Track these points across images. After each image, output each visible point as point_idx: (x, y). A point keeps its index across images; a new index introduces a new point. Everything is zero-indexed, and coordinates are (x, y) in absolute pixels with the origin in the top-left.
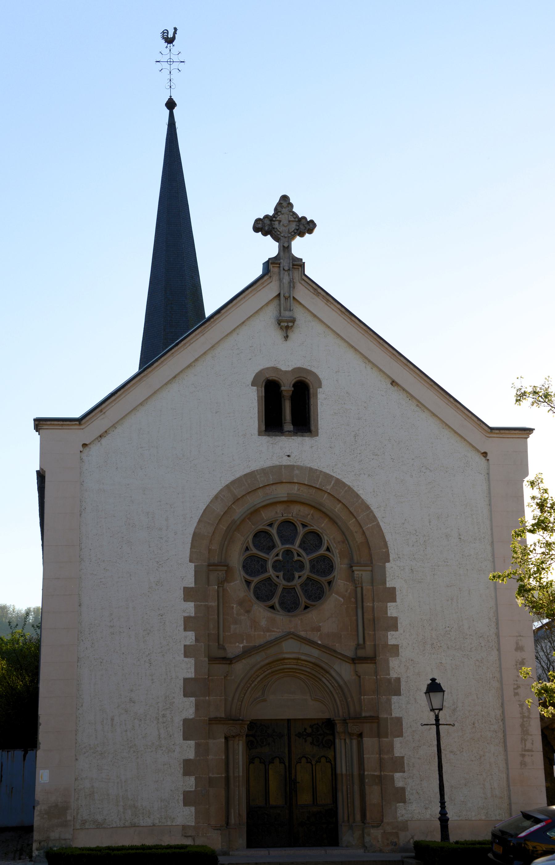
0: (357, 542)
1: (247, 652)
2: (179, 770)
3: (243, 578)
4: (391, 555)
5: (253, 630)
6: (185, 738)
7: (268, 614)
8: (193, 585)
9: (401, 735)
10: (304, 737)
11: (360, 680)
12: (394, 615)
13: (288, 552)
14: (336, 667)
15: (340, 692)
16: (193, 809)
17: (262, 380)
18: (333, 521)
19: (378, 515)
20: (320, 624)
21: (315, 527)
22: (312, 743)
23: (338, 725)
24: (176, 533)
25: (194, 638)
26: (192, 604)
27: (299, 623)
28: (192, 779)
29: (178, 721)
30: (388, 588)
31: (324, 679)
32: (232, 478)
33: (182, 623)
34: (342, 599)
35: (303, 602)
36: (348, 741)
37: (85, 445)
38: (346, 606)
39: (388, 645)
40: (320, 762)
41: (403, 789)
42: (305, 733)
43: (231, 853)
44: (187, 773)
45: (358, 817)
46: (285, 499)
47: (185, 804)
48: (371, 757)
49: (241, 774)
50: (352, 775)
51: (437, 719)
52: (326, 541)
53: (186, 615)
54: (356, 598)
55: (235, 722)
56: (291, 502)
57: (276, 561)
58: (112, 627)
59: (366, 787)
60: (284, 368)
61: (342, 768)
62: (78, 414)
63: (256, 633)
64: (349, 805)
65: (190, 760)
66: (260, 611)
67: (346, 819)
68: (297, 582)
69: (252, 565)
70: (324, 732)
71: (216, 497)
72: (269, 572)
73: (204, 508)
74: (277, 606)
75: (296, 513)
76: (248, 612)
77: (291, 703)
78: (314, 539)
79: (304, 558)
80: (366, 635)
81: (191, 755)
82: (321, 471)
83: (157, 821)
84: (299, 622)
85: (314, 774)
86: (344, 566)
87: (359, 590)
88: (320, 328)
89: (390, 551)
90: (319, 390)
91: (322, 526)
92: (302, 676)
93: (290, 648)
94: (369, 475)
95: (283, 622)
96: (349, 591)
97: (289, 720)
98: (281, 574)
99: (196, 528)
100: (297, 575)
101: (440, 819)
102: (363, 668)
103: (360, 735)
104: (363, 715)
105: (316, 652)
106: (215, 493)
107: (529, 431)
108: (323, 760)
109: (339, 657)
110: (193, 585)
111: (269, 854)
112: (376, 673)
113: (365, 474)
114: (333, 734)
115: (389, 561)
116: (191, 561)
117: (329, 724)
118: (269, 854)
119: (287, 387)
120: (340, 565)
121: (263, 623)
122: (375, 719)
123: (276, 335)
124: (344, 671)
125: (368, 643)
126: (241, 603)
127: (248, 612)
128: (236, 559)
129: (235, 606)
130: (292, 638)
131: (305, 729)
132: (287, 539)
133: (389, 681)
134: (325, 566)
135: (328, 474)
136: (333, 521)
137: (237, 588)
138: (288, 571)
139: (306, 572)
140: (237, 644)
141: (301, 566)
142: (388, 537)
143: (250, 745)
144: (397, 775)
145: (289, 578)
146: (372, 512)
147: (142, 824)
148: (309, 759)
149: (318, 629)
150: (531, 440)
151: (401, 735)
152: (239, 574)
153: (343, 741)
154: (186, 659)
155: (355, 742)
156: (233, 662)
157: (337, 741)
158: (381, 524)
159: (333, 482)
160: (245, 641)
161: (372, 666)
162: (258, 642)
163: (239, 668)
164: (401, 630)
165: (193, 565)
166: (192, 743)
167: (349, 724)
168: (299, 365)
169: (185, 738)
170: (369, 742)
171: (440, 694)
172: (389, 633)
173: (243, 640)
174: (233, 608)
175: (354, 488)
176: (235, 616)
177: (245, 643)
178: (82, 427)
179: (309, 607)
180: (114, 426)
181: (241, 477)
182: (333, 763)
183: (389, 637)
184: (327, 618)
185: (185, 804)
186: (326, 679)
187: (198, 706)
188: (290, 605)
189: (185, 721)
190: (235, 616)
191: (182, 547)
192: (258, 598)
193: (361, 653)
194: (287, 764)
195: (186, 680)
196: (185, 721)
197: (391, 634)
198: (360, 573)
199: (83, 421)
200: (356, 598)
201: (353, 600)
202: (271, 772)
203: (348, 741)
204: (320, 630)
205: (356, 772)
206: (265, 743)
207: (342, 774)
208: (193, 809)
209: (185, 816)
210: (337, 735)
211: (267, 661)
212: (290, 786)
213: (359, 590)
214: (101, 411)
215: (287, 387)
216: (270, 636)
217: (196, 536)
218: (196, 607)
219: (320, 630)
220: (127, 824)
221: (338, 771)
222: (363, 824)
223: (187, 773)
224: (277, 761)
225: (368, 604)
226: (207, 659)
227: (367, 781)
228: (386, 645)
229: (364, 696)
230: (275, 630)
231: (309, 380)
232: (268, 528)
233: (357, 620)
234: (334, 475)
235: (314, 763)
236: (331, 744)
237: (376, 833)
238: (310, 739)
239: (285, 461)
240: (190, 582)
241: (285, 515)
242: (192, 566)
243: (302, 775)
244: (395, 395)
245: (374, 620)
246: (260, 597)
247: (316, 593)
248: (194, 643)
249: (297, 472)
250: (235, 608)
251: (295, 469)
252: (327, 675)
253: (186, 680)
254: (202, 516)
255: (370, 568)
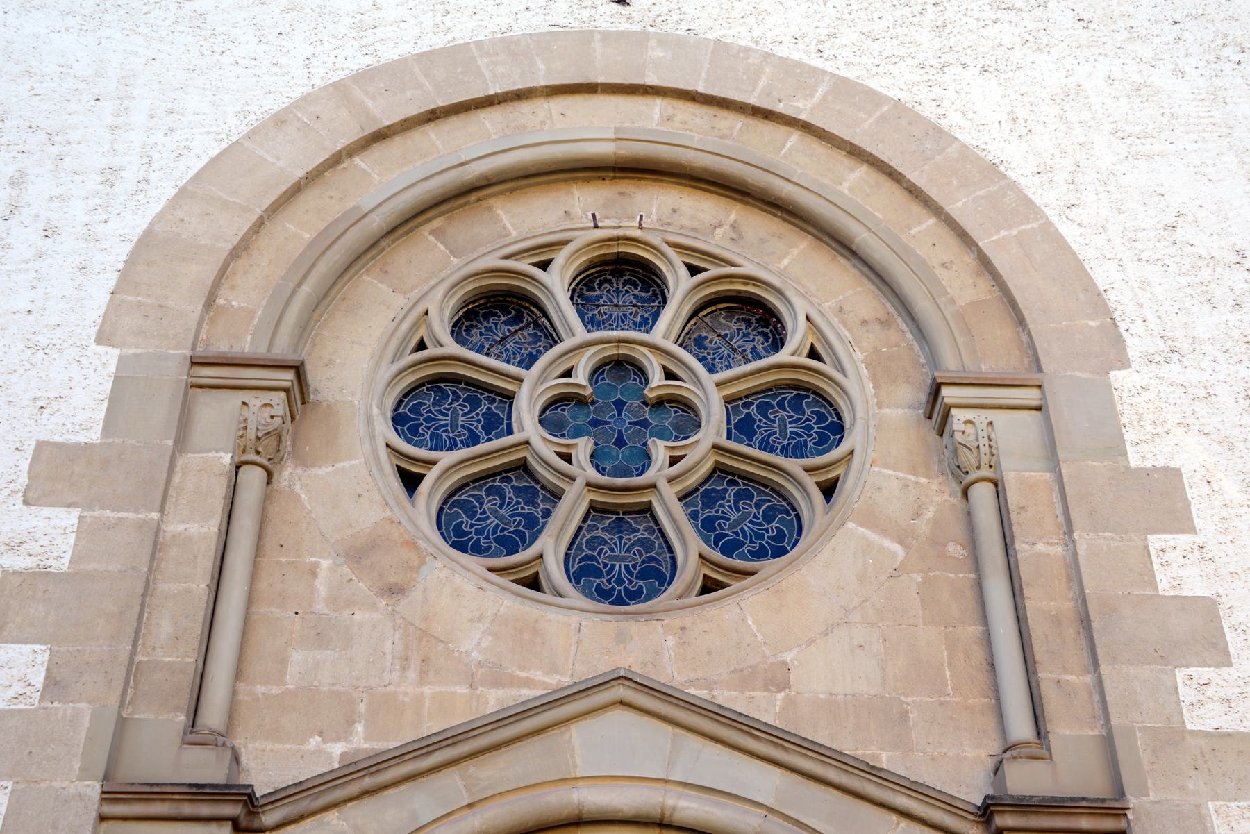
0: (953, 301)
3: (383, 453)
4: (1130, 341)
5: (412, 674)
7: (508, 602)
12: (1195, 586)
13: (621, 368)
18: (840, 244)
20: (788, 657)
21: (748, 269)
24: (50, 232)
25: (39, 679)
27: (670, 641)
30: (1138, 470)
34: (897, 548)
35: (694, 559)
38: (918, 577)
39: (1183, 731)
52: (802, 319)
54: (973, 544)
57: (558, 401)
63: (427, 690)
66: (463, 593)
69: (434, 403)
72: (522, 429)
73: (216, 152)
74: (554, 569)
76: (395, 591)
79: (698, 381)
82: (767, 56)
84: (671, 641)
89: (1122, 327)
94: (984, 70)
95: (576, 637)
96: (929, 514)
98: (583, 447)
99: (159, 217)
100: (660, 450)
109: (902, 801)
113: (964, 66)
115: (1124, 363)
125: (1062, 731)
126: (358, 554)
128: (360, 369)
129: (325, 564)
130: (622, 703)
135: (800, 65)
137: (350, 481)
138: (620, 442)
140: (315, 741)
141: (683, 415)
146: (1013, 185)
149: (778, 679)
159: (820, 93)
160: (359, 727)
165: (111, 356)
172: (1180, 674)
173: (350, 722)
174: (313, 572)
175: (918, 108)
176: (320, 607)
179: (720, 585)
181: (403, 61)
183: (1187, 694)
188: (621, 566)
190: (320, 607)
197: (1188, 680)
198: (981, 417)
200: (973, 544)
201: (956, 550)
204: (784, 685)
213: (983, 494)
219: (784, 685)
225: (1041, 547)
226: (93, 789)
228: (1173, 736)
230: (538, 675)
232: (537, 272)
233: (987, 640)
234: (829, 67)
240: (82, 416)
241: (607, 223)
245: (1085, 621)
246: (462, 528)
250: (323, 574)
251: (653, 43)
254: (197, 177)
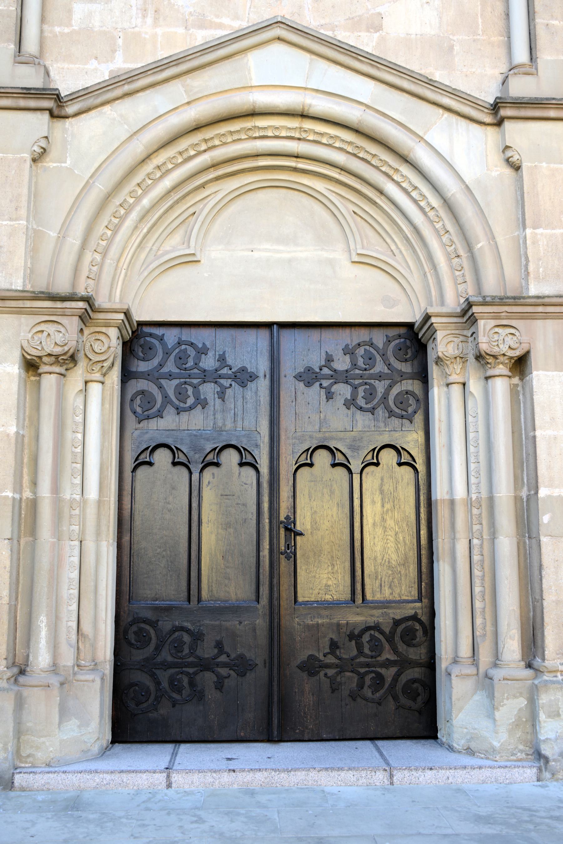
1: (122, 87)
10: (325, 383)
11: (520, 180)
14: (436, 137)
15: (449, 227)
22: (350, 403)
23: (439, 335)
31: (390, 188)
36: (475, 386)
40: (377, 464)
42: (326, 371)
43: (18, 779)
45: (512, 647)
49: (92, 493)
50: (491, 499)
55: (59, 304)
59: (544, 540)
61: (452, 480)
63: (159, 31)
64: (478, 605)
67: (465, 651)
80: (541, 32)
85: (357, 502)
92: (320, 185)
103: (521, 364)
104: (533, 290)
108: (388, 458)
111: (169, 786)
114: (423, 377)
117: (413, 340)
118: (169, 786)
131: (329, 359)
143: (134, 406)
148: (338, 455)
153: (456, 390)
156: (70, 109)
157: (437, 392)
163: (92, 137)
167: (481, 323)
173: (114, 51)
182: (420, 466)
186: (398, 184)
193: (521, 87)
194: (264, 469)
202: (208, 495)
203: (475, 386)
204: (378, 28)
205: (504, 490)
206: (191, 401)
207: (452, 502)
210: (434, 372)
212: (281, 536)
219: (378, 28)
221: (440, 492)
222: (529, 673)
224: (230, 458)
227: (545, 519)
229: (535, 228)
235: (356, 466)
236: (418, 408)
238: (343, 391)
243: (317, 505)
252: (405, 169)
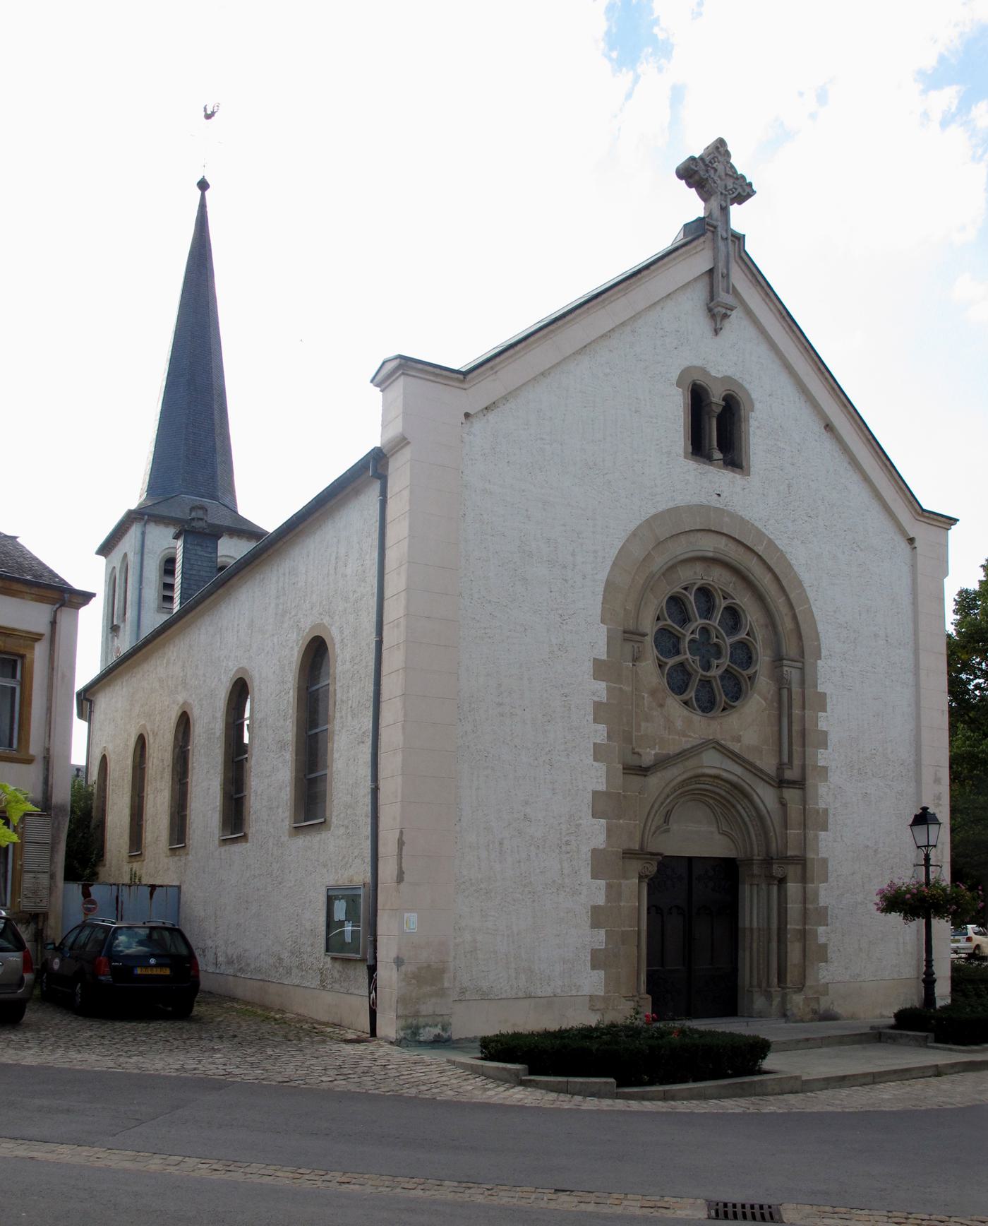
2: (586, 921)
6: (595, 876)
7: (685, 712)
8: (604, 657)
9: (826, 881)
13: (705, 630)
16: (602, 973)
17: (688, 382)
19: (811, 595)
21: (737, 601)
24: (584, 577)
26: (603, 685)
28: (602, 932)
29: (585, 852)
32: (653, 511)
33: (590, 710)
36: (764, 886)
37: (467, 415)
41: (825, 946)
44: (595, 925)
46: (711, 554)
47: (594, 967)
48: (793, 907)
50: (769, 929)
51: (927, 858)
53: (596, 699)
56: (672, 568)
57: (692, 641)
58: (500, 704)
60: (713, 373)
62: (459, 361)
65: (598, 907)
66: (673, 704)
68: (715, 673)
70: (727, 872)
71: (634, 534)
75: (717, 578)
76: (661, 706)
77: (698, 837)
78: (734, 616)
81: (601, 901)
83: (559, 991)
86: (767, 659)
87: (785, 692)
88: (751, 331)
90: (752, 414)
91: (744, 600)
93: (712, 762)
97: (690, 859)
101: (924, 981)
102: (791, 794)
105: (738, 770)
106: (633, 527)
107: (953, 521)
110: (604, 657)
112: (804, 802)
116: (603, 621)
119: (716, 397)
120: (763, 658)
121: (679, 724)
122: (801, 861)
123: (702, 324)
124: (766, 796)
126: (653, 693)
127: (661, 706)
128: (649, 626)
132: (708, 612)
133: (818, 811)
134: (745, 654)
136: (760, 597)
139: (725, 661)
142: (820, 627)
144: (821, 929)
145: (707, 667)
147: (540, 994)
150: (954, 532)
151: (826, 881)
152: (651, 651)
154: (596, 764)
155: (775, 888)
158: (814, 609)
161: (797, 791)
162: (673, 749)
164: (830, 749)
166: (602, 883)
168: (729, 373)
169: (595, 876)
170: (793, 888)
171: (936, 827)
177: (657, 750)
178: (466, 386)
180: (505, 398)
184: (748, 725)
185: (594, 967)
187: (610, 831)
188: (707, 704)
189: (595, 852)
191: (590, 601)
192: (672, 690)
195: (595, 793)
196: (595, 852)
199: (470, 376)
205: (774, 926)
207: (752, 929)
208: (602, 973)
209: (592, 982)
211: (685, 776)
213: (785, 692)
214: (492, 368)
215: (716, 397)
216: (686, 743)
217: (609, 586)
218: (609, 690)
220: (521, 994)
223: (595, 925)
226: (621, 767)
228: (816, 767)
231: (741, 396)
237: (797, 999)
239: (714, 502)
240: (601, 652)
242: (604, 628)
244: (828, 444)
247: (736, 690)
248: (605, 742)
249: (727, 519)
253: (595, 793)
255: (799, 665)
